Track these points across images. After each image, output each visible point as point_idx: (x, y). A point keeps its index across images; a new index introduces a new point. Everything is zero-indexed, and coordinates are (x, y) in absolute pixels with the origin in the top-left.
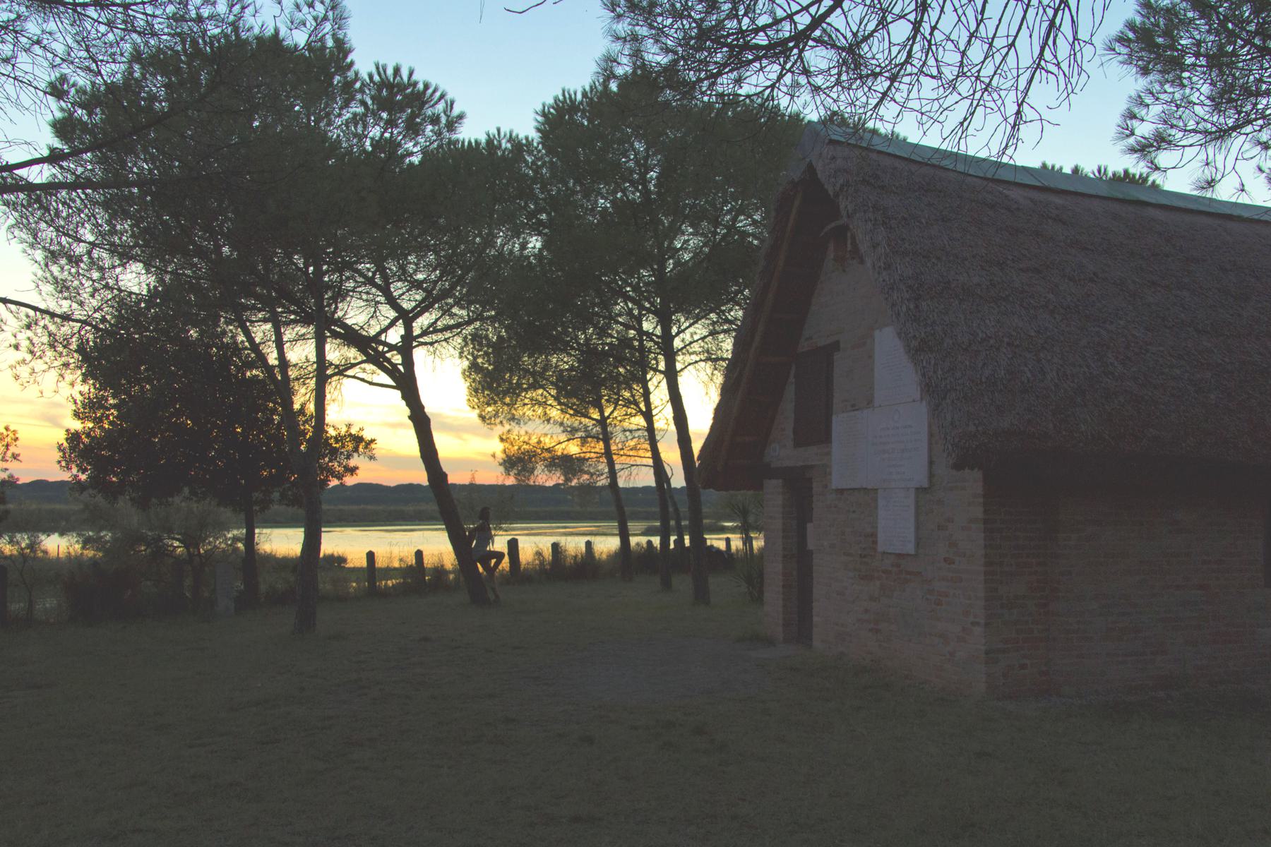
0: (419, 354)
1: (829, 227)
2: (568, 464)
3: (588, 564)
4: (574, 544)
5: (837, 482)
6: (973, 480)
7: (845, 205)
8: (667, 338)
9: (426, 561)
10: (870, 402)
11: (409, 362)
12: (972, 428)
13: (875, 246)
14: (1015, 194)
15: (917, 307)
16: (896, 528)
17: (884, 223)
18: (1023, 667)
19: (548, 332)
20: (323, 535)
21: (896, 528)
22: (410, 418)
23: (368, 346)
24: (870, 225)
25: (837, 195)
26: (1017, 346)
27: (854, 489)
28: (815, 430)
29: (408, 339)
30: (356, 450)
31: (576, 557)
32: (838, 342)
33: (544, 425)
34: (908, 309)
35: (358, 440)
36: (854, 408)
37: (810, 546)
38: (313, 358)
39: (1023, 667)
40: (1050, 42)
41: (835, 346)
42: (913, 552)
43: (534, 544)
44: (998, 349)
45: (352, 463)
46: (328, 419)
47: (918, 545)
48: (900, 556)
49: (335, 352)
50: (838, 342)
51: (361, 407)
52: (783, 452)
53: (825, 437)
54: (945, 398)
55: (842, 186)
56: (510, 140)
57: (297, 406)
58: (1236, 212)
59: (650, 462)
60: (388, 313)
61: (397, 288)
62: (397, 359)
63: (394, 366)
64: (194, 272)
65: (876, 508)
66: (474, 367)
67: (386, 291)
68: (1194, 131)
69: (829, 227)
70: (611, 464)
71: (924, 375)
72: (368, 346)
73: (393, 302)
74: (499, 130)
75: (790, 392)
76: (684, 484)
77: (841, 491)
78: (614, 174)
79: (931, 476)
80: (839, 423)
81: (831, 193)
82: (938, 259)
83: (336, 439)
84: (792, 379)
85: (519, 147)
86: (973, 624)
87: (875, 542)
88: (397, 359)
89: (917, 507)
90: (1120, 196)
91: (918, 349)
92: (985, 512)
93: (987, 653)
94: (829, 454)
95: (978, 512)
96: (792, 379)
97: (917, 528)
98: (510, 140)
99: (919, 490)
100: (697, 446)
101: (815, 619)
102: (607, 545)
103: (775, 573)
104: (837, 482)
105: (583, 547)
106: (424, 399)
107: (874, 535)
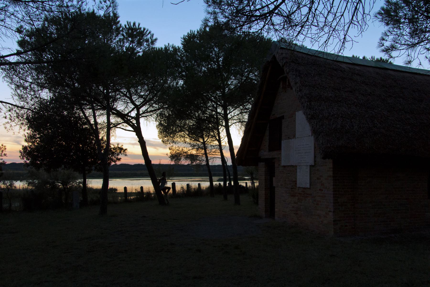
0: (142, 120)
2: (192, 157)
3: (199, 191)
4: (194, 185)
5: (283, 163)
6: (329, 163)
7: (286, 69)
8: (226, 115)
9: (144, 190)
10: (294, 136)
11: (138, 123)
12: (329, 145)
13: (296, 83)
14: (343, 66)
15: (310, 104)
16: (303, 179)
18: (346, 226)
19: (185, 113)
21: (303, 179)
23: (125, 117)
24: (294, 76)
25: (283, 66)
27: (289, 166)
28: (276, 145)
31: (195, 189)
33: (184, 144)
34: (307, 104)
35: (121, 149)
36: (289, 138)
39: (346, 226)
40: (355, 14)
41: (283, 117)
42: (309, 187)
43: (181, 184)
45: (119, 157)
46: (145, 139)
47: (310, 185)
50: (283, 116)
51: (122, 137)
52: (265, 153)
53: (279, 148)
54: (319, 135)
55: (285, 63)
56: (173, 47)
57: (100, 138)
59: (220, 156)
61: (134, 98)
62: (134, 122)
64: (66, 92)
65: (296, 172)
66: (160, 124)
68: (404, 44)
70: (207, 157)
71: (312, 127)
73: (133, 102)
74: (169, 44)
75: (267, 133)
76: (231, 164)
77: (284, 167)
78: (208, 59)
80: (284, 143)
81: (281, 65)
82: (318, 88)
83: (114, 149)
85: (176, 50)
86: (329, 211)
87: (296, 184)
88: (134, 122)
91: (310, 118)
93: (334, 221)
94: (280, 154)
95: (331, 173)
97: (310, 179)
98: (173, 47)
99: (311, 166)
100: (236, 151)
101: (276, 210)
102: (205, 185)
103: (262, 193)
104: (283, 163)
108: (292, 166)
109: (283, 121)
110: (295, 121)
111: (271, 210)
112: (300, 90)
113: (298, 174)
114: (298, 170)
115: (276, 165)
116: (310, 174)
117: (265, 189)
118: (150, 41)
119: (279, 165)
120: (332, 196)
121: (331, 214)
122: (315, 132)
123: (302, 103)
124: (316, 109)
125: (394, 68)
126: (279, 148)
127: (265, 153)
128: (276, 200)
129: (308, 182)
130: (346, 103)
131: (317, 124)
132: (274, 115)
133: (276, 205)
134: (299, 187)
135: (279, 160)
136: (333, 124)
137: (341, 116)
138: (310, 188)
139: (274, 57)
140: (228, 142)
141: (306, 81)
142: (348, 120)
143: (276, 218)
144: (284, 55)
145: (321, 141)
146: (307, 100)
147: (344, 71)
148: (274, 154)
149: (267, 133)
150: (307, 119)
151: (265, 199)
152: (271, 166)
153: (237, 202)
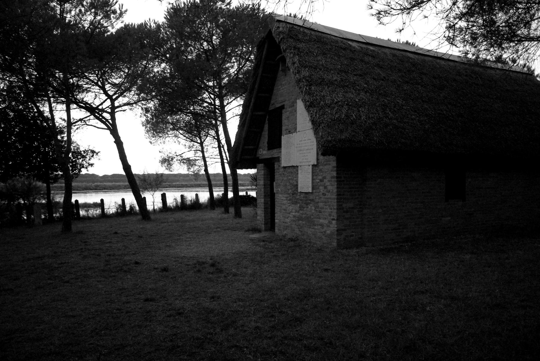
0: (118, 115)
1: (279, 57)
2: (189, 162)
3: (196, 205)
4: (190, 196)
5: (284, 163)
6: (332, 161)
7: (283, 46)
8: (222, 106)
10: (295, 129)
11: (113, 118)
12: (330, 138)
13: (294, 63)
14: (354, 44)
15: (310, 89)
16: (305, 182)
17: (298, 54)
18: (352, 236)
19: (176, 105)
20: (73, 195)
21: (305, 182)
22: (122, 143)
23: (92, 110)
24: (292, 55)
25: (280, 42)
26: (350, 105)
27: (289, 167)
29: (113, 108)
30: (93, 156)
31: (191, 201)
32: (284, 105)
33: (176, 145)
34: (306, 89)
35: (93, 152)
36: (290, 132)
37: (275, 191)
38: (205, 153)
39: (352, 236)
41: (283, 107)
42: (311, 191)
43: (173, 197)
44: (342, 107)
45: (91, 162)
48: (306, 193)
49: (77, 113)
50: (284, 105)
51: (88, 136)
52: (264, 153)
54: (319, 126)
55: (281, 39)
56: (155, 23)
58: (451, 58)
59: (220, 160)
60: (104, 97)
61: (107, 87)
62: (107, 116)
63: (107, 120)
65: (298, 174)
67: (103, 88)
69: (279, 57)
70: (205, 162)
71: (311, 117)
72: (92, 110)
73: (106, 93)
75: (266, 127)
77: (285, 167)
78: (197, 37)
79: (318, 159)
80: (284, 139)
81: (277, 42)
82: (321, 69)
83: (84, 152)
84: (267, 122)
85: (158, 26)
87: (297, 188)
88: (107, 116)
89: (313, 173)
90: (397, 48)
91: (309, 107)
92: (337, 174)
93: (337, 231)
94: (281, 152)
95: (334, 174)
96: (267, 122)
97: (313, 183)
98: (155, 23)
101: (276, 221)
102: (204, 196)
103: (261, 201)
104: (284, 163)
105: (194, 197)
106: (120, 134)
107: (297, 185)
108: (293, 167)
109: (283, 111)
110: (296, 111)
111: (271, 223)
112: (299, 72)
113: (300, 175)
114: (299, 171)
115: (276, 166)
116: (313, 176)
117: (265, 196)
118: (118, 12)
119: (279, 166)
120: (336, 201)
121: (334, 222)
122: (316, 124)
123: (300, 88)
124: (317, 95)
125: (413, 50)
126: (279, 146)
127: (264, 153)
128: (277, 210)
129: (311, 185)
130: (353, 89)
131: (316, 112)
132: (274, 104)
133: (276, 215)
134: (301, 192)
135: (278, 159)
136: (336, 112)
137: (347, 104)
138: (312, 193)
139: (270, 32)
140: (226, 141)
141: (306, 61)
142: (354, 109)
143: (276, 230)
144: (281, 29)
145: (320, 134)
146: (305, 84)
147: (355, 51)
148: (274, 153)
149: (266, 127)
150: (305, 108)
151: (264, 208)
152: (270, 166)
153: (238, 214)
